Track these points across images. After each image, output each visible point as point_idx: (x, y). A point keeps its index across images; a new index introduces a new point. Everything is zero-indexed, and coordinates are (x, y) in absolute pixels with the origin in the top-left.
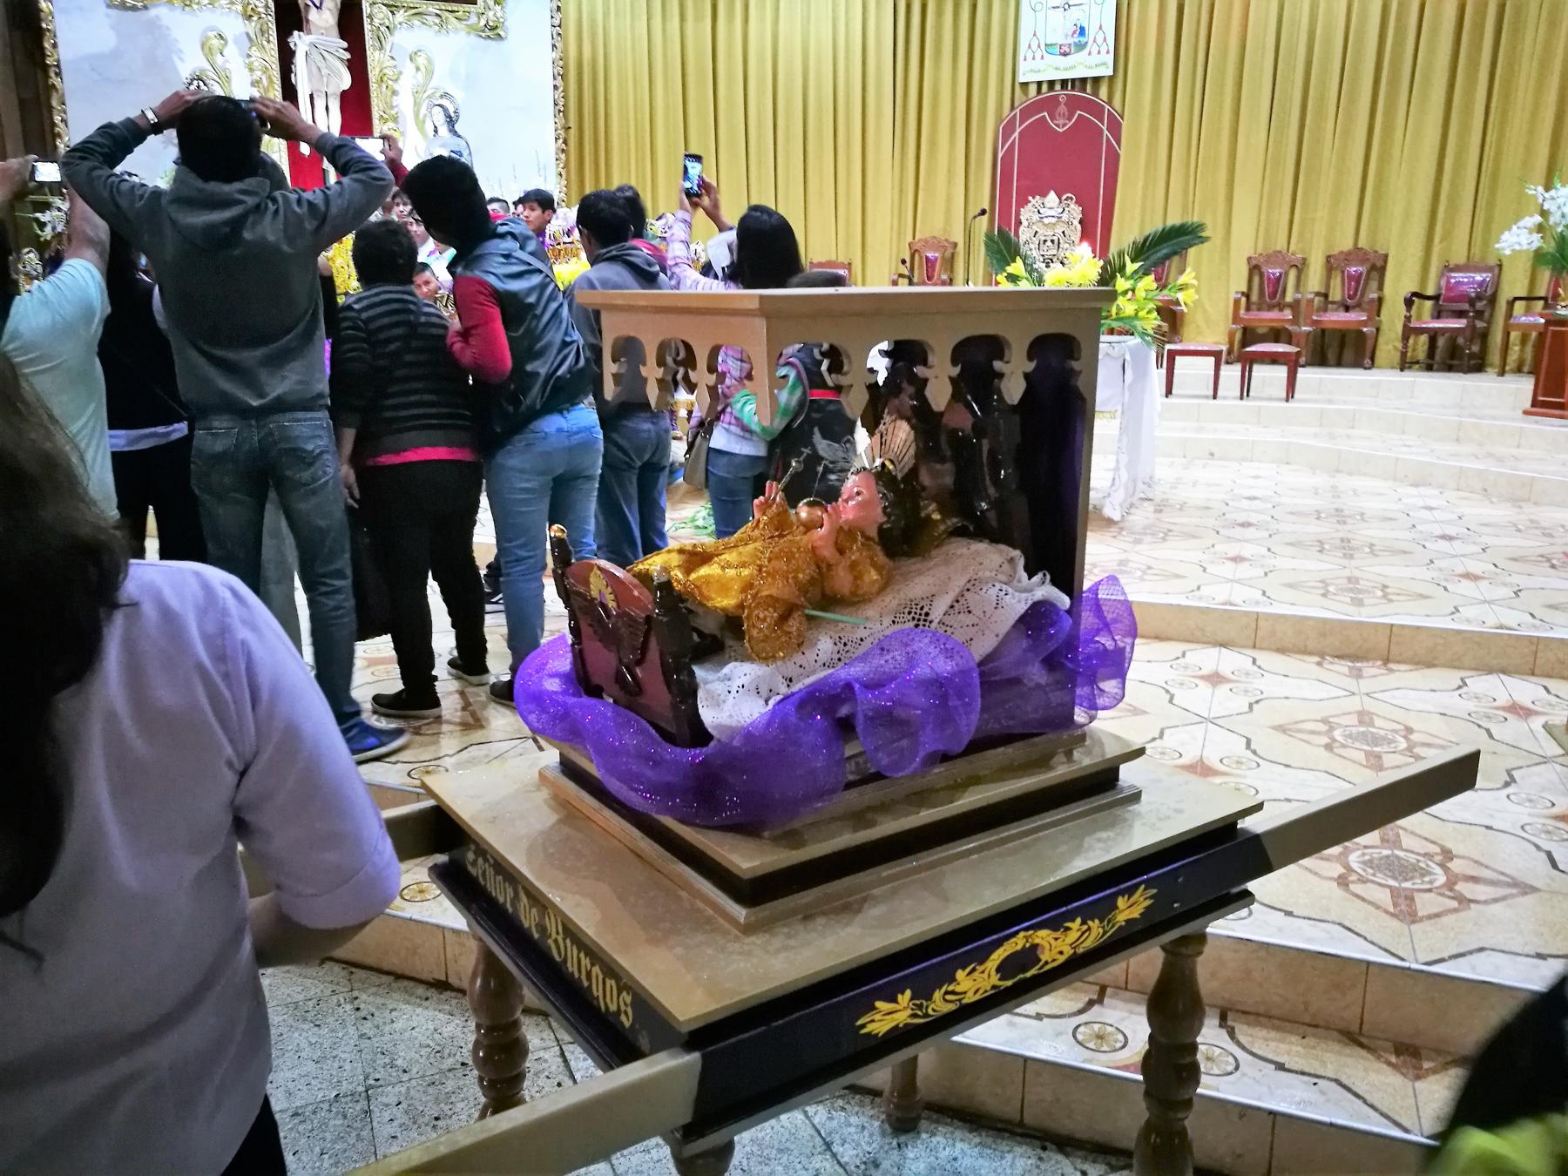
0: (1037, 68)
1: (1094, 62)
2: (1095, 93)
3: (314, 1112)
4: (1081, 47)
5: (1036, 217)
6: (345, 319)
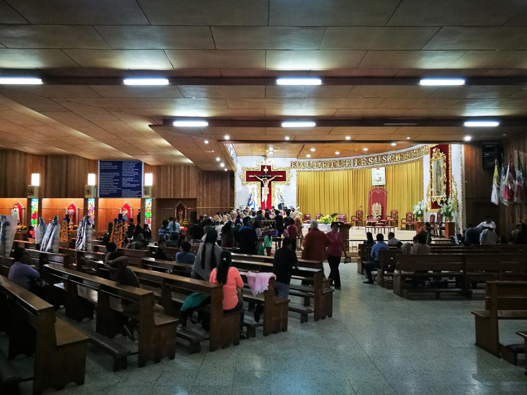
0: (375, 183)
1: (383, 182)
2: (384, 187)
3: (211, 374)
4: (380, 180)
5: (374, 207)
6: (101, 239)
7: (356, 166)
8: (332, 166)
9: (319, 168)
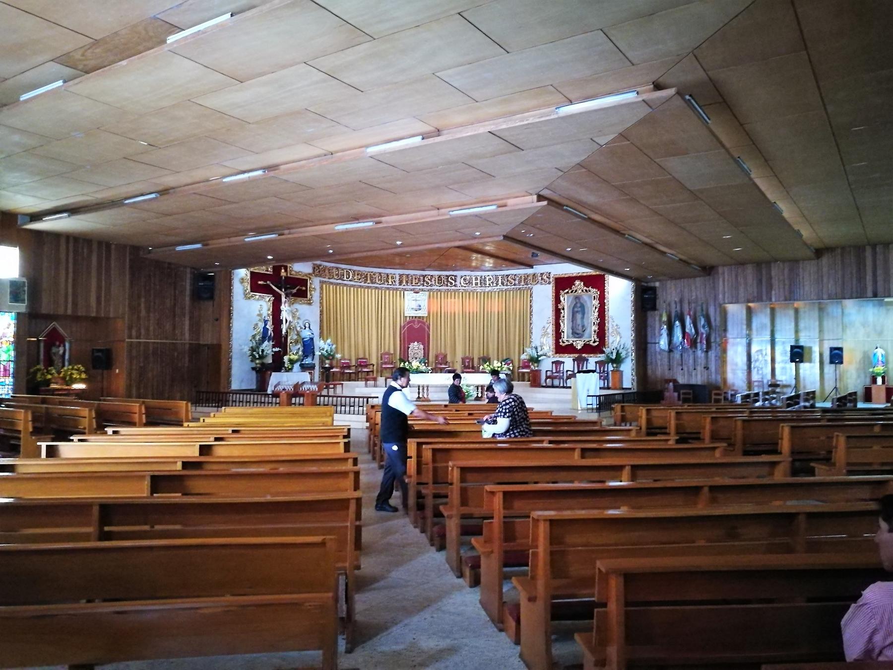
0: (409, 313)
2: (423, 319)
4: (420, 309)
7: (404, 285)
8: (523, 283)
9: (350, 280)
